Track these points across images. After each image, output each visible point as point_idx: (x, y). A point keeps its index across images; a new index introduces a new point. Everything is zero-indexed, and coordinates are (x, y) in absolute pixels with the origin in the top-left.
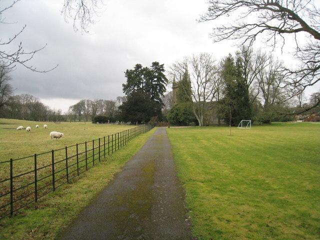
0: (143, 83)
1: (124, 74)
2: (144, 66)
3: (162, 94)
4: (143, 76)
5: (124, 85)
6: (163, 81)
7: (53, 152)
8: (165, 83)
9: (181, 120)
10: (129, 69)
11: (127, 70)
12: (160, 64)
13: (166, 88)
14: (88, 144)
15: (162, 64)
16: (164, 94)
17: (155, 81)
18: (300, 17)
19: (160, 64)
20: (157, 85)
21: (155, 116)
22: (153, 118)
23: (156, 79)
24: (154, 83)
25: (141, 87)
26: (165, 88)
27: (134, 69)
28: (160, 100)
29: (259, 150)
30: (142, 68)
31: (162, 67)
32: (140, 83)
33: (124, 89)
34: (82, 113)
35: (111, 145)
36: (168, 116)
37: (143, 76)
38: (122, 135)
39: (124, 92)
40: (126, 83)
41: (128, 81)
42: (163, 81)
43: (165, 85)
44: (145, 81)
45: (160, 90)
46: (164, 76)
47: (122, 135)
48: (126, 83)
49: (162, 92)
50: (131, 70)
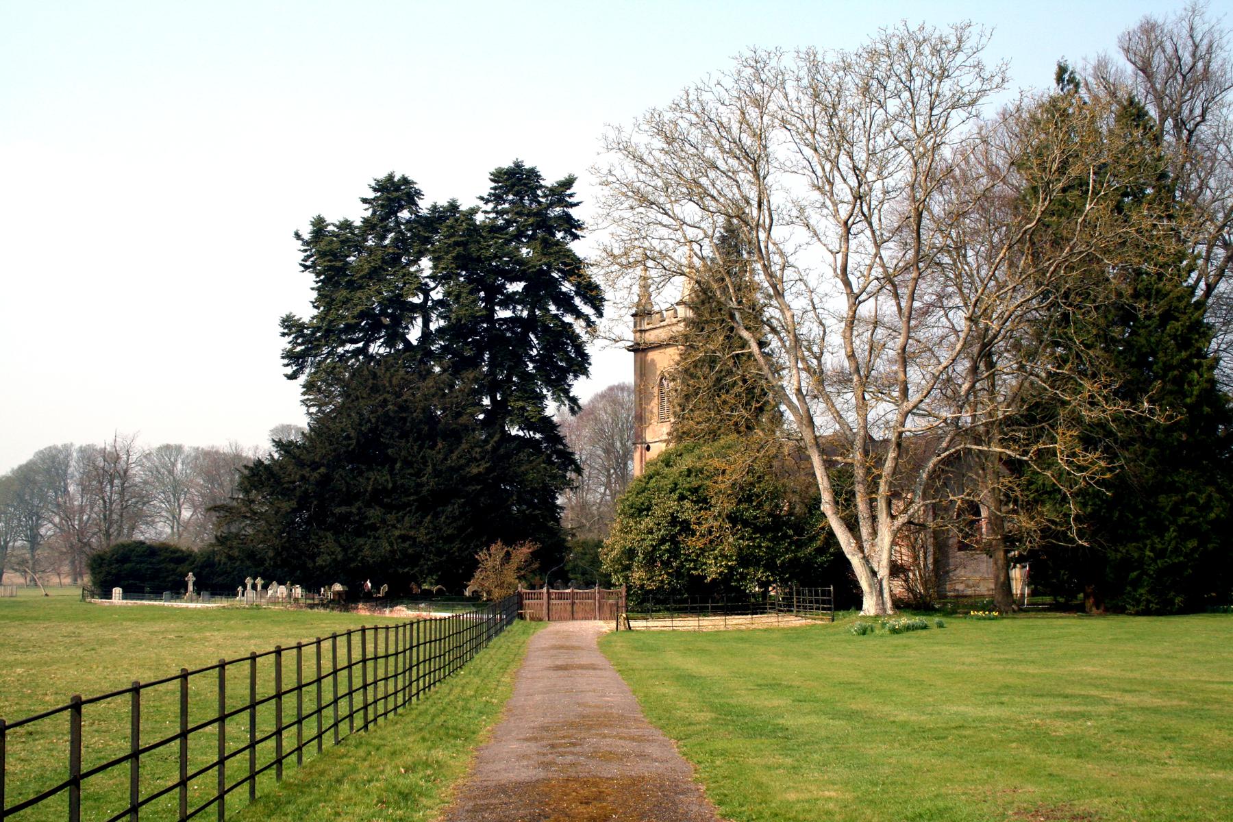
0: (424, 310)
1: (296, 253)
2: (432, 197)
3: (562, 391)
4: (426, 264)
5: (290, 325)
6: (565, 303)
7: (136, 690)
8: (579, 314)
9: (712, 570)
10: (333, 218)
11: (319, 226)
12: (550, 178)
13: (588, 349)
14: (322, 644)
15: (562, 177)
16: (582, 389)
17: (509, 301)
18: (6, 789)
19: (550, 178)
20: (530, 324)
21: (511, 540)
22: (498, 550)
23: (517, 287)
24: (503, 314)
25: (414, 335)
26: (579, 349)
27: (358, 214)
28: (547, 426)
29: (572, 725)
30: (424, 206)
31: (561, 201)
32: (401, 311)
33: (291, 356)
34: (46, 530)
35: (203, 749)
36: (613, 543)
37: (426, 264)
38: (415, 659)
39: (292, 377)
40: (306, 313)
41: (325, 298)
42: (565, 303)
43: (579, 327)
44: (437, 294)
45: (544, 363)
46: (574, 267)
47: (415, 659)
48: (306, 313)
49: (562, 378)
50: (346, 225)
